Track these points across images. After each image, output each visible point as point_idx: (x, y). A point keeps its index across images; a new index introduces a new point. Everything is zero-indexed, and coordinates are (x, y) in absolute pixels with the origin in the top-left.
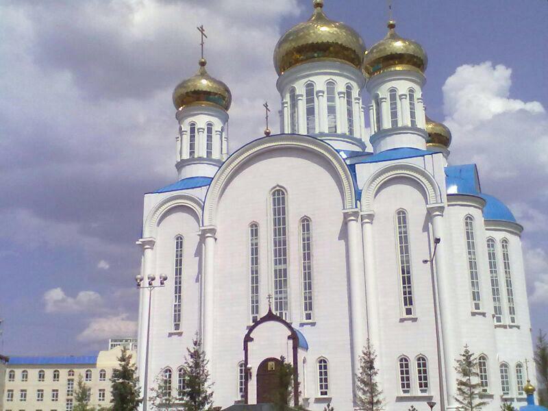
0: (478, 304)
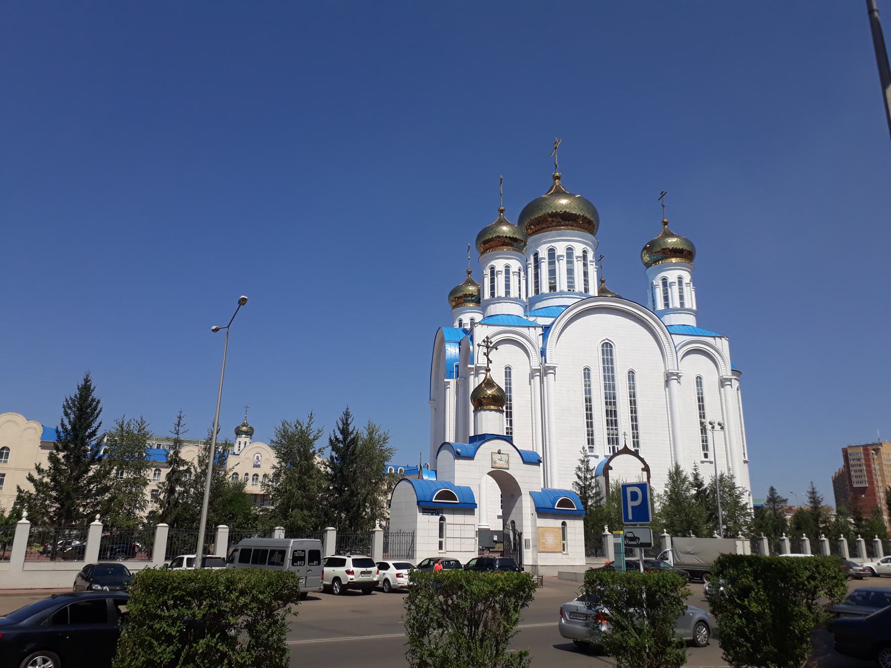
0: (707, 454)
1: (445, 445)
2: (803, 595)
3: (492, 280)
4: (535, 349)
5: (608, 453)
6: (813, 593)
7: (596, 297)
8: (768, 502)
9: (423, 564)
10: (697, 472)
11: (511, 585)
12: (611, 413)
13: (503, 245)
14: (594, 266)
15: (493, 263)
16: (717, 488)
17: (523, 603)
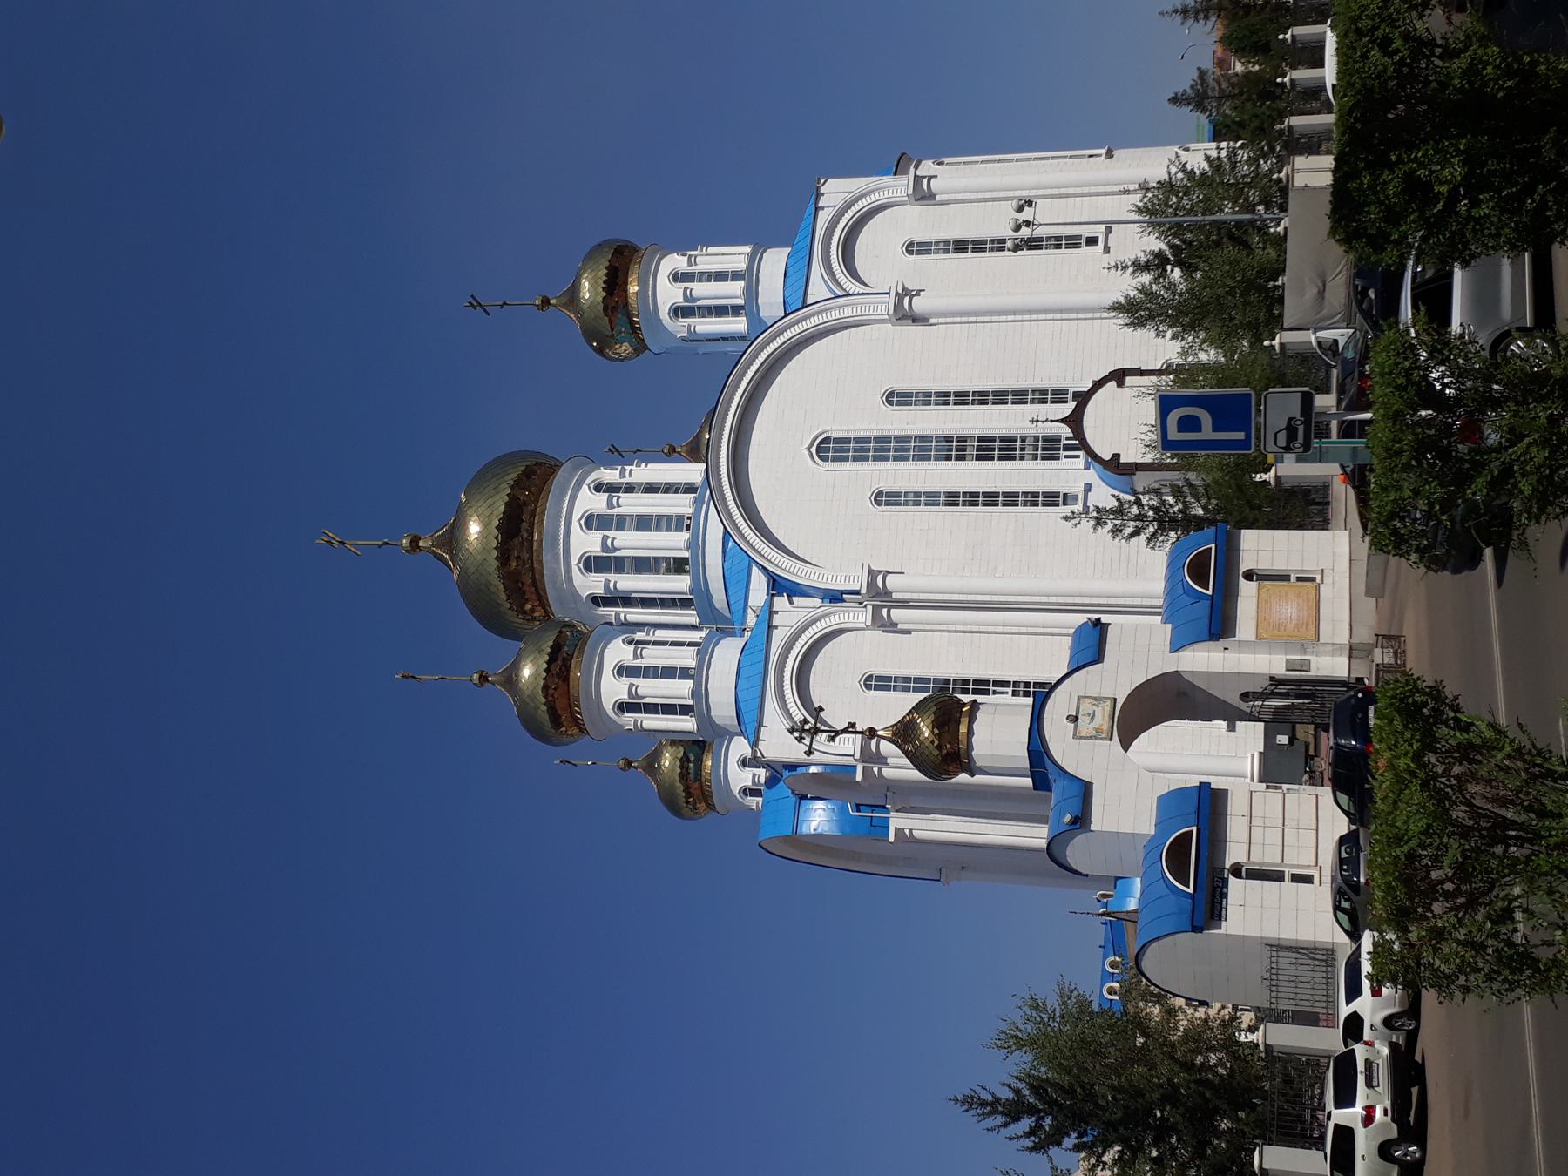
1: (1056, 851)
2: (1424, 66)
3: (652, 709)
4: (824, 616)
5: (1080, 462)
6: (1421, 45)
7: (707, 469)
8: (1204, 110)
9: (1347, 927)
10: (1129, 263)
11: (1408, 735)
12: (984, 450)
13: (566, 679)
14: (634, 467)
15: (608, 705)
16: (1170, 223)
17: (1451, 707)
